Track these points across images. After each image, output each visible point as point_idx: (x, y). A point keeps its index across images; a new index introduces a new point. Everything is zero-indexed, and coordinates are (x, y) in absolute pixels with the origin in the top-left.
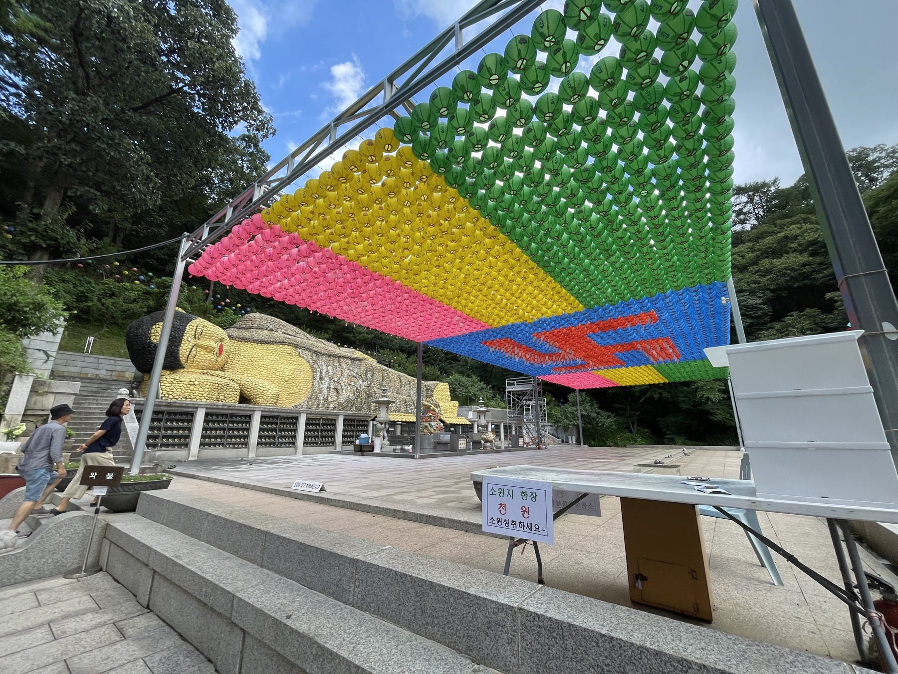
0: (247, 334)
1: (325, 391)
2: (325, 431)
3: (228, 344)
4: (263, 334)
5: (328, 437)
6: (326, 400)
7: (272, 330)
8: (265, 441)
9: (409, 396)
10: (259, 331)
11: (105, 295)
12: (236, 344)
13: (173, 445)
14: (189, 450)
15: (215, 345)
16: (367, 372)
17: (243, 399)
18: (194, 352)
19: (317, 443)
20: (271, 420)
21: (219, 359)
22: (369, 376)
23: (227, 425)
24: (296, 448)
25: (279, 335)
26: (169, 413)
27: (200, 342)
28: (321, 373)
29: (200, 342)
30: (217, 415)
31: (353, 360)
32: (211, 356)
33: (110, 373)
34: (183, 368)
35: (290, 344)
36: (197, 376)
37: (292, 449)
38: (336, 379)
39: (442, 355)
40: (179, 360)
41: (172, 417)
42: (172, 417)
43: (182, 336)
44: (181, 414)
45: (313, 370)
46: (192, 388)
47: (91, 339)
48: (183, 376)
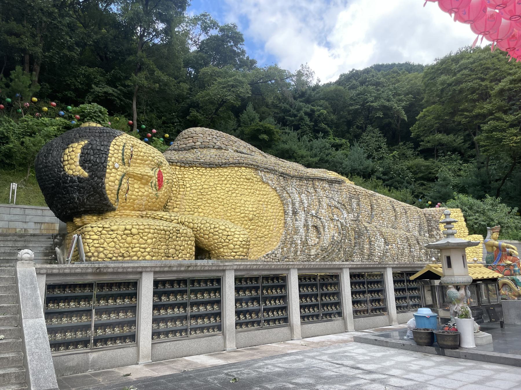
0: (190, 156)
1: (302, 231)
2: (326, 295)
3: (167, 170)
4: (210, 155)
5: (331, 304)
6: (305, 243)
7: (220, 148)
8: (245, 319)
9: (408, 231)
10: (205, 151)
11: (24, 134)
12: (178, 172)
13: (114, 339)
14: (137, 345)
15: (151, 173)
16: (350, 198)
17: (201, 252)
18: (125, 186)
19: (317, 316)
21: (160, 193)
22: (355, 205)
23: (189, 296)
24: (292, 330)
25: (230, 154)
26: (101, 286)
28: (293, 204)
29: (130, 169)
31: (331, 182)
32: (148, 190)
33: (38, 226)
34: (114, 210)
35: (248, 166)
36: (135, 221)
37: (284, 331)
39: (410, 175)
40: (106, 199)
41: (106, 291)
42: (106, 291)
43: (106, 161)
44: (119, 285)
45: (284, 203)
46: (129, 239)
47: (14, 186)
48: (116, 223)
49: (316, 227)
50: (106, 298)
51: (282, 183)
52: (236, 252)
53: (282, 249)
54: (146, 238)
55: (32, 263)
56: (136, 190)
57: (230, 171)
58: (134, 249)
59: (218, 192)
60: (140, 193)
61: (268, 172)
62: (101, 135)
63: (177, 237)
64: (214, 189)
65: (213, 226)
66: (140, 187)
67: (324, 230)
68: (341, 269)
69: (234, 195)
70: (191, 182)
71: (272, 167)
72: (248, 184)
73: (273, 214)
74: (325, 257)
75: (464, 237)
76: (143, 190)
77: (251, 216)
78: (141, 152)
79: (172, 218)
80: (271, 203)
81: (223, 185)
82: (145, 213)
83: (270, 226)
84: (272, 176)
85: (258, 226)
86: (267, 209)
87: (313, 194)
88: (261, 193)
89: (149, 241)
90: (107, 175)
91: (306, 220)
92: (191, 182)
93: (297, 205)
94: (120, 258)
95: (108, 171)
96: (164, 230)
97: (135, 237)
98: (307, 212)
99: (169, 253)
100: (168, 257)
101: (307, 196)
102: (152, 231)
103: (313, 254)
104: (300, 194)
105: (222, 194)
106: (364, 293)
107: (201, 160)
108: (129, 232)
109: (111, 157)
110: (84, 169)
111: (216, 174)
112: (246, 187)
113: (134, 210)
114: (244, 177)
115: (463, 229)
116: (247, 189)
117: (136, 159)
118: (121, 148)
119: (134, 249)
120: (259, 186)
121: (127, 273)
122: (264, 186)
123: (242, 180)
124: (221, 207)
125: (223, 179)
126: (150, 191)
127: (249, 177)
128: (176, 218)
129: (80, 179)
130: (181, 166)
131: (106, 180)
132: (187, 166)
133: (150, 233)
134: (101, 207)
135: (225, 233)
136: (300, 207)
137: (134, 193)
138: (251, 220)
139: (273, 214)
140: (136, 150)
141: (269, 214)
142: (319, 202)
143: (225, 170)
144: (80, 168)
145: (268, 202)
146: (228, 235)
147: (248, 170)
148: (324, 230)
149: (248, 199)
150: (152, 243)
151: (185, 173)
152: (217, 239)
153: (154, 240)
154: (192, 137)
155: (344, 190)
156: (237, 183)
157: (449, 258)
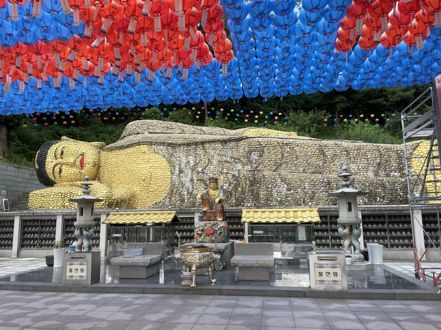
1: (188, 184)
20: (398, 220)
30: (374, 216)
32: (75, 170)
34: (55, 183)
38: (200, 169)
41: (393, 219)
42: (393, 219)
50: (393, 223)
68: (56, 216)
76: (71, 171)
77: (144, 178)
84: (162, 147)
87: (202, 155)
95: (46, 164)
98: (193, 169)
102: (53, 194)
106: (327, 231)
112: (142, 158)
122: (157, 155)
126: (76, 170)
136: (186, 166)
138: (144, 180)
156: (137, 157)
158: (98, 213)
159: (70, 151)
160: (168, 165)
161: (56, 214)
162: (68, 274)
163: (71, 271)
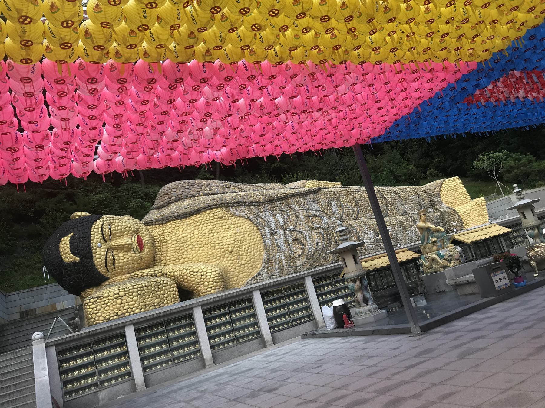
0: (166, 212)
4: (185, 205)
6: (289, 258)
7: (193, 196)
12: (156, 231)
25: (202, 200)
27: (112, 243)
29: (112, 243)
31: (304, 194)
32: (130, 256)
34: (107, 279)
35: (218, 206)
37: (195, 363)
38: (291, 227)
43: (90, 243)
46: (119, 301)
49: (296, 240)
51: (254, 211)
52: (211, 288)
53: (267, 269)
54: (132, 296)
55: (43, 340)
56: (121, 258)
57: (203, 216)
58: (125, 308)
59: (196, 236)
60: (125, 260)
61: (238, 206)
62: (82, 224)
63: (159, 288)
64: (192, 235)
65: (188, 271)
66: (124, 255)
67: (306, 240)
69: (212, 234)
70: (171, 235)
71: (241, 200)
72: (222, 222)
73: (252, 241)
74: (311, 265)
75: (467, 203)
76: (127, 256)
77: (230, 249)
78: (118, 226)
79: (156, 272)
80: (247, 231)
81: (200, 229)
82: (133, 274)
83: (251, 252)
84: (242, 208)
85: (240, 255)
86: (245, 238)
87: (288, 211)
88: (236, 225)
89: (135, 298)
90: (94, 255)
91: (286, 237)
92: (171, 235)
93: (273, 226)
94: (115, 317)
95: (93, 251)
96: (146, 286)
97: (123, 298)
98: (284, 229)
99: (154, 303)
100: (155, 306)
101: (282, 215)
102: (135, 290)
103: (299, 264)
104: (274, 215)
105: (200, 237)
107: (176, 214)
108: (117, 295)
109: (93, 240)
110: (75, 254)
111: (191, 222)
113: (124, 274)
114: (217, 217)
115: (465, 196)
116: (222, 226)
117: (116, 234)
118: (100, 229)
119: (125, 308)
120: (234, 220)
121: (98, 334)
123: (215, 220)
124: (202, 249)
125: (199, 224)
126: (134, 255)
127: (220, 215)
128: (160, 271)
129: (74, 263)
130: (159, 224)
131: (94, 259)
132: (164, 222)
133: (134, 292)
134: (98, 280)
135: (199, 274)
137: (120, 261)
138: (231, 252)
139: (252, 241)
140: (113, 226)
141: (248, 241)
142: (297, 216)
143: (199, 216)
144: (72, 255)
145: (244, 232)
146: (202, 276)
147: (219, 209)
148: (306, 240)
149: (225, 235)
150: (138, 299)
151: (164, 229)
152: (194, 281)
153: (139, 296)
154: (167, 194)
155: (322, 197)
156: (212, 224)
157: (344, 259)
158: (120, 325)
159: (119, 228)
160: (255, 228)
161: (251, 290)
162: (496, 285)
163: (497, 281)
